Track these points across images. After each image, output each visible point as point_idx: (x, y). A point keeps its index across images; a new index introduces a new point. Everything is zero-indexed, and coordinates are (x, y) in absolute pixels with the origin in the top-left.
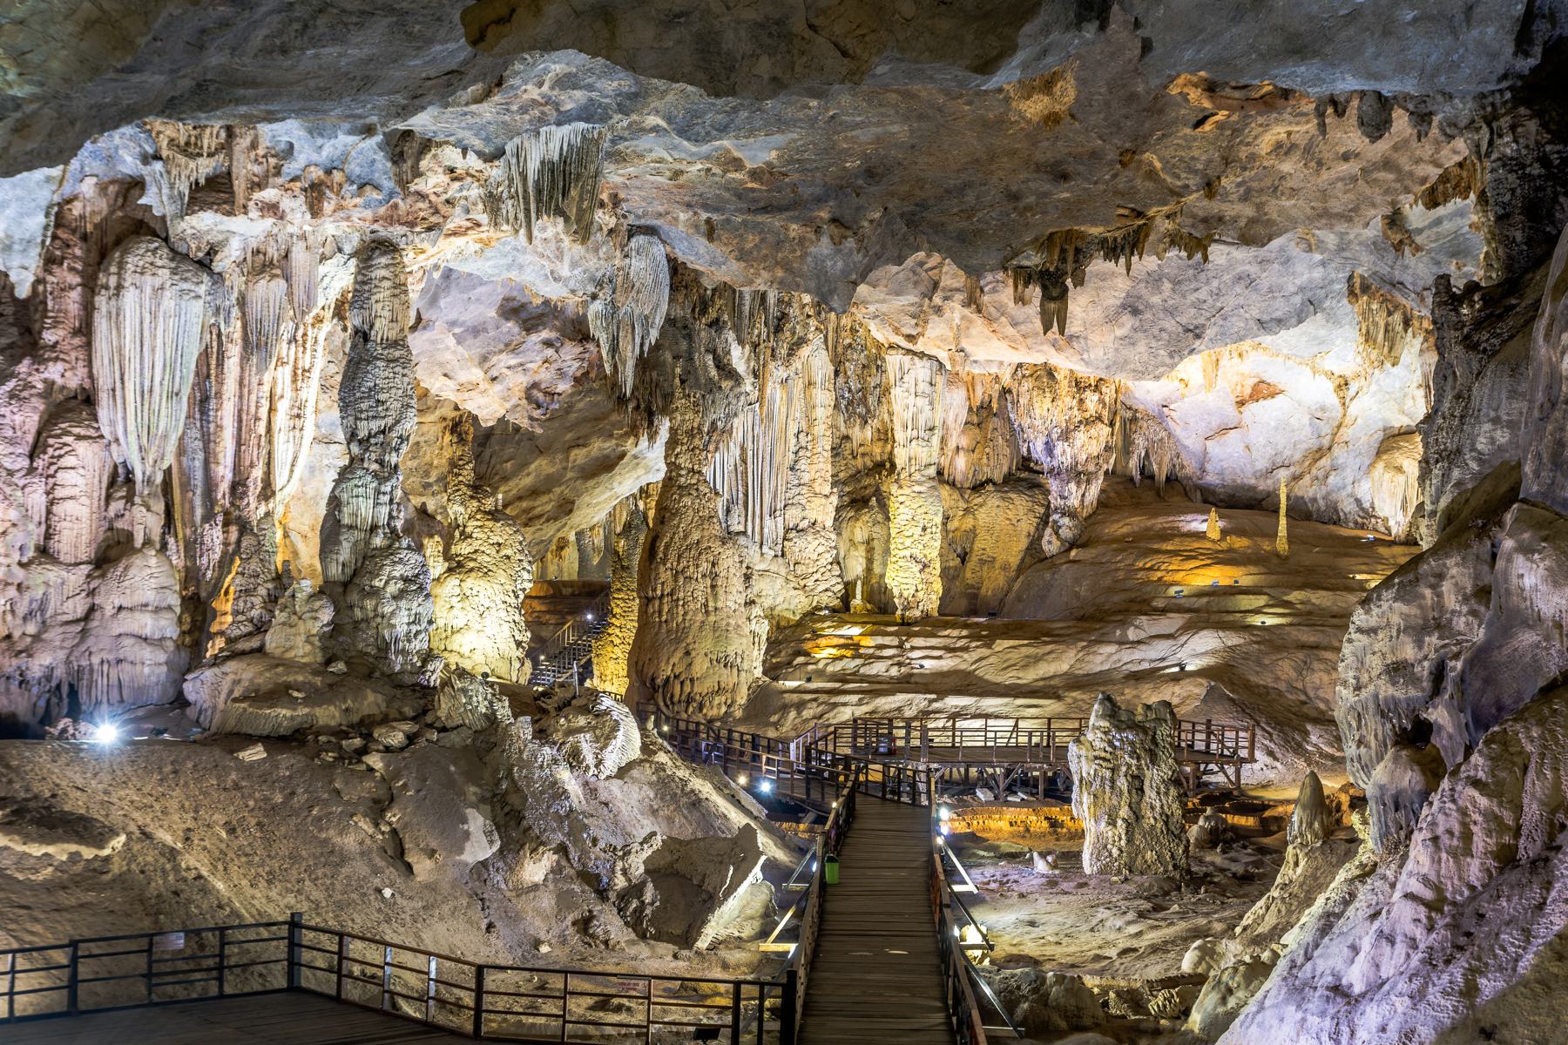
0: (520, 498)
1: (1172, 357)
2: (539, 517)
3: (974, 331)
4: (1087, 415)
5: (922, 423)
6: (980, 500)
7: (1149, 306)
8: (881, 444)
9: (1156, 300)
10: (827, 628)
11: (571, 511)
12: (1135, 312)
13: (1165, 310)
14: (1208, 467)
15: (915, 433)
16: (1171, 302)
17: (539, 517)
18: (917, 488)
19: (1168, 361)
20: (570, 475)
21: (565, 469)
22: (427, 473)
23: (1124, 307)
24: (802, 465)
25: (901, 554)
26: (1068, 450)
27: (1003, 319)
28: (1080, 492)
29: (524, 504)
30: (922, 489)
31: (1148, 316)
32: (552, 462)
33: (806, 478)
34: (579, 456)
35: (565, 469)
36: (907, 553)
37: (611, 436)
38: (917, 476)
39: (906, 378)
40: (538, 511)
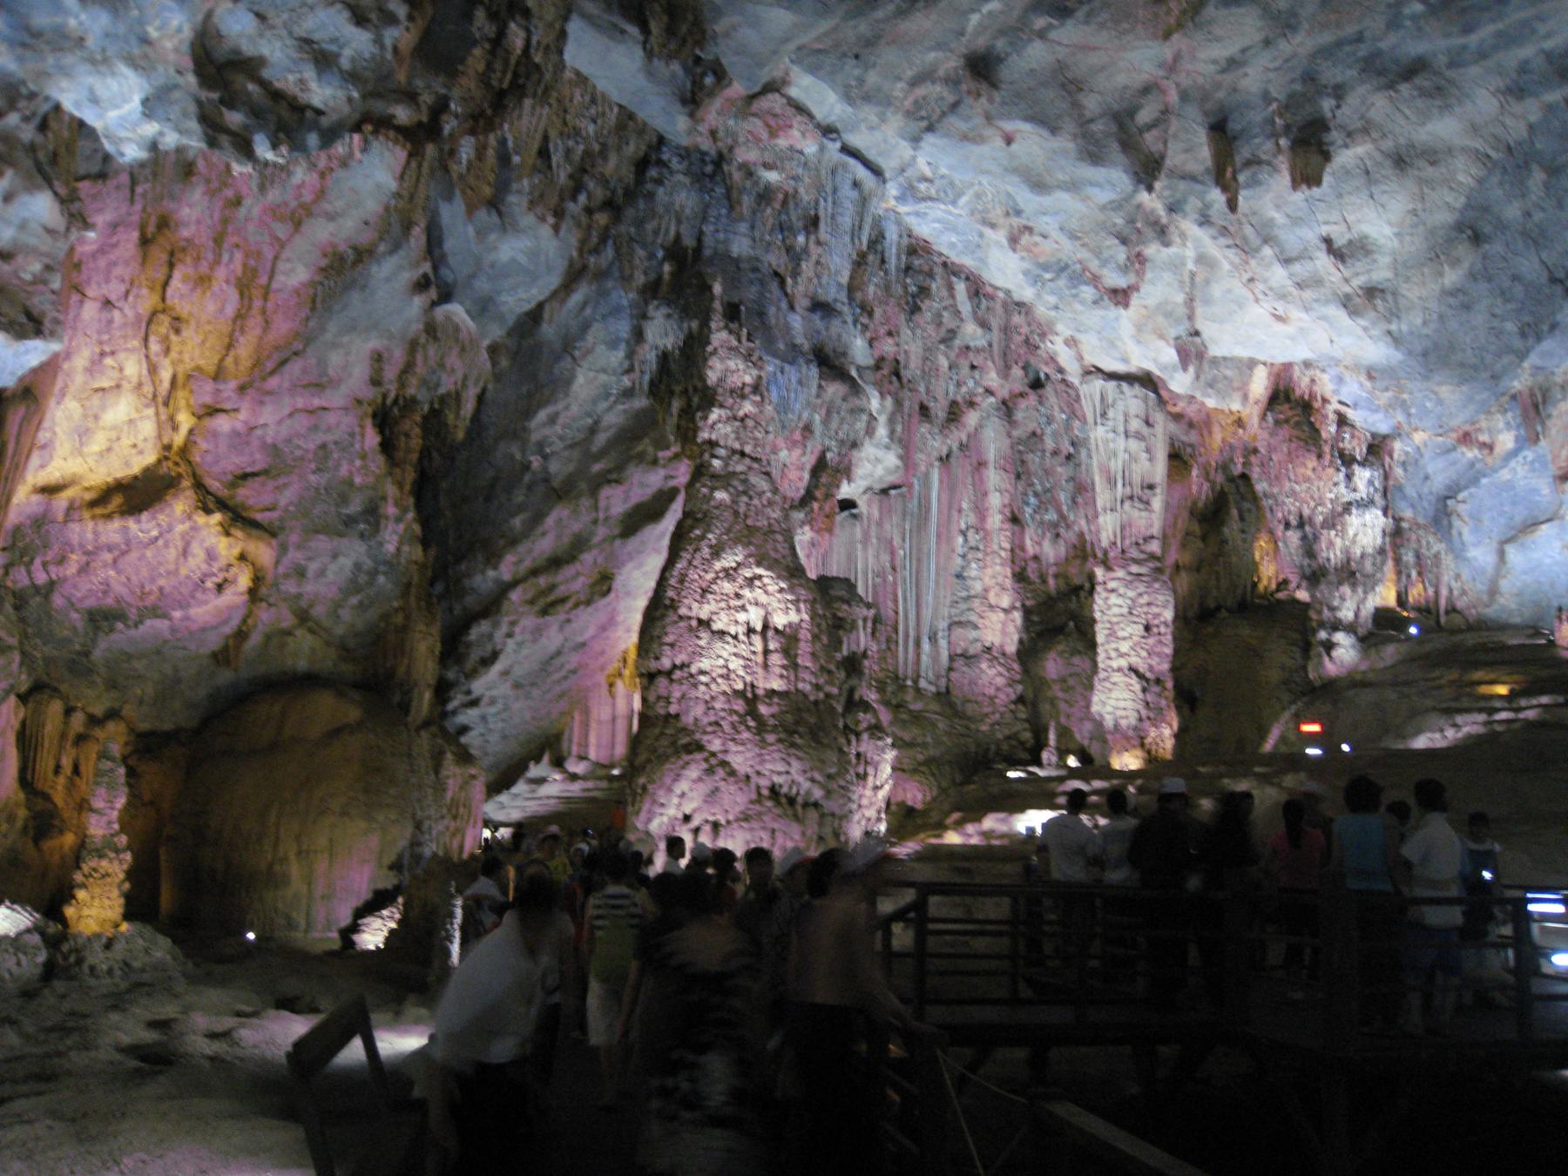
0: (534, 572)
1: (1523, 335)
2: (563, 600)
3: (1216, 290)
4: (1357, 496)
5: (1137, 479)
6: (1210, 629)
7: (1501, 226)
8: (1078, 562)
9: (1512, 212)
10: (568, 117)
11: (609, 590)
12: (1477, 239)
13: (1525, 234)
14: (1504, 584)
15: (1128, 490)
16: (1538, 216)
17: (563, 600)
18: (1135, 569)
19: (1518, 343)
20: (601, 532)
21: (595, 522)
22: (344, 499)
23: (1459, 227)
24: (973, 570)
25: (1115, 664)
26: (1338, 542)
27: (1267, 251)
28: (1356, 598)
29: (542, 581)
30: (1143, 570)
31: (1496, 248)
32: (575, 513)
33: (977, 587)
34: (617, 500)
35: (595, 522)
36: (1123, 663)
37: (655, 462)
38: (1134, 553)
39: (1111, 414)
40: (560, 591)
